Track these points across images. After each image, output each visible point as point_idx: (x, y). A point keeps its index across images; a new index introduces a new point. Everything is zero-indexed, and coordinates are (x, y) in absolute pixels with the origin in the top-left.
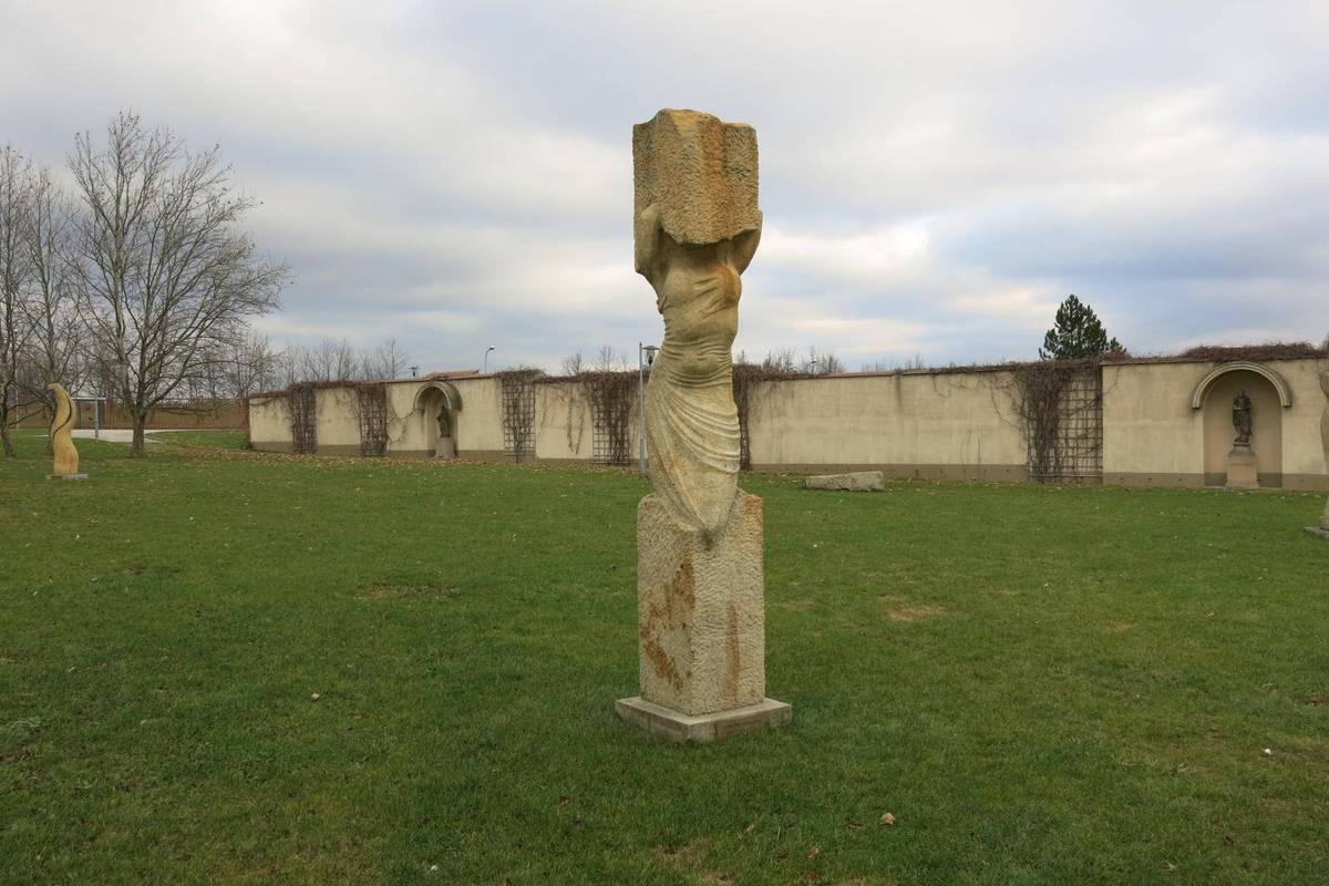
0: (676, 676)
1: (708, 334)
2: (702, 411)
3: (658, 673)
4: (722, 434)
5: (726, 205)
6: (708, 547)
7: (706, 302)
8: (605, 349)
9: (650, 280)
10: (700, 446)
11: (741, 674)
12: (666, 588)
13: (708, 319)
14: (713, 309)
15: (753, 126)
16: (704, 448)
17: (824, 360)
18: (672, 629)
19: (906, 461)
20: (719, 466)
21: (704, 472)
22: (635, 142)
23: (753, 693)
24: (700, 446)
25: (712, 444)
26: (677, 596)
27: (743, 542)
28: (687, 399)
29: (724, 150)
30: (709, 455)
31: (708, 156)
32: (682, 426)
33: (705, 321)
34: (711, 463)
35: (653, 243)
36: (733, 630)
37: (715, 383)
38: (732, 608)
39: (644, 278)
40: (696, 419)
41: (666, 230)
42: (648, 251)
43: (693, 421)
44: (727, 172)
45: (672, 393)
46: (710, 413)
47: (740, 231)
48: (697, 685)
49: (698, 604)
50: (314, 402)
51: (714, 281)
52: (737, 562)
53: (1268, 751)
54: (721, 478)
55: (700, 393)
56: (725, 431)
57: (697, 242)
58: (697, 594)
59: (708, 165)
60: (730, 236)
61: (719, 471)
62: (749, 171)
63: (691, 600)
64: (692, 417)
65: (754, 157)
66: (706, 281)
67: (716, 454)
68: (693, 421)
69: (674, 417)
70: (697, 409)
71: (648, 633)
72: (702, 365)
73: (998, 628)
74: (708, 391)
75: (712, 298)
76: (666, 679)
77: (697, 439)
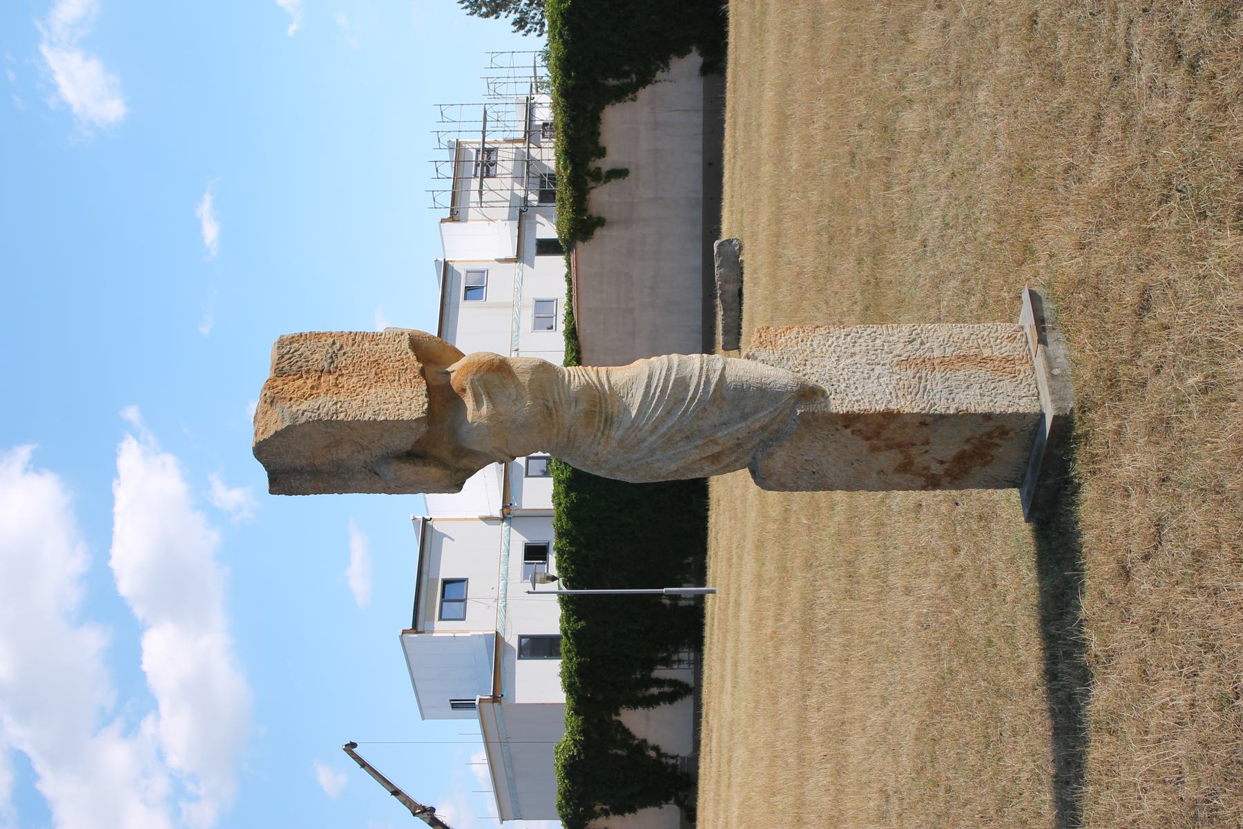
0: (990, 435)
3: (987, 463)
5: (378, 370)
6: (818, 291)
9: (471, 472)
12: (874, 449)
15: (276, 339)
17: (1082, 723)
18: (927, 443)
22: (290, 492)
23: (1012, 338)
26: (886, 434)
32: (663, 430)
35: (425, 465)
39: (468, 481)
41: (409, 448)
42: (434, 472)
47: (411, 354)
50: (664, 754)
62: (334, 343)
65: (318, 336)
71: (934, 475)
73: (743, 710)
76: (994, 452)
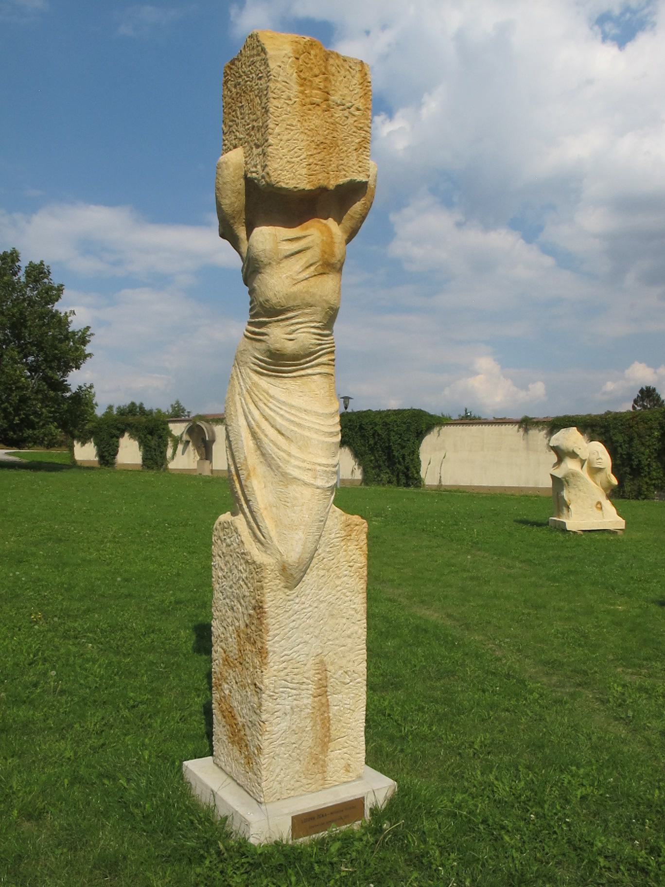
1: (298, 307)
2: (292, 406)
4: (315, 436)
7: (296, 266)
8: (568, 485)
10: (284, 451)
11: (332, 745)
13: (299, 287)
14: (305, 274)
16: (289, 455)
19: (531, 485)
20: (306, 477)
21: (286, 486)
24: (284, 451)
25: (300, 448)
26: (248, 647)
27: (339, 578)
28: (273, 391)
29: (326, 79)
30: (297, 463)
31: (303, 82)
32: (265, 425)
33: (295, 289)
34: (295, 473)
36: (322, 690)
37: (309, 371)
38: (322, 662)
40: (282, 416)
43: (278, 419)
44: (329, 106)
45: (255, 384)
46: (299, 409)
48: (270, 764)
49: (272, 658)
51: (310, 239)
52: (331, 603)
53: (608, 795)
54: (307, 492)
55: (289, 384)
56: (317, 431)
57: (284, 185)
58: (269, 646)
59: (302, 92)
60: (332, 184)
61: (305, 484)
63: (262, 653)
64: (278, 414)
66: (298, 239)
67: (304, 461)
68: (278, 419)
69: (256, 413)
70: (284, 403)
72: (290, 347)
74: (299, 381)
75: (305, 260)
77: (280, 440)
